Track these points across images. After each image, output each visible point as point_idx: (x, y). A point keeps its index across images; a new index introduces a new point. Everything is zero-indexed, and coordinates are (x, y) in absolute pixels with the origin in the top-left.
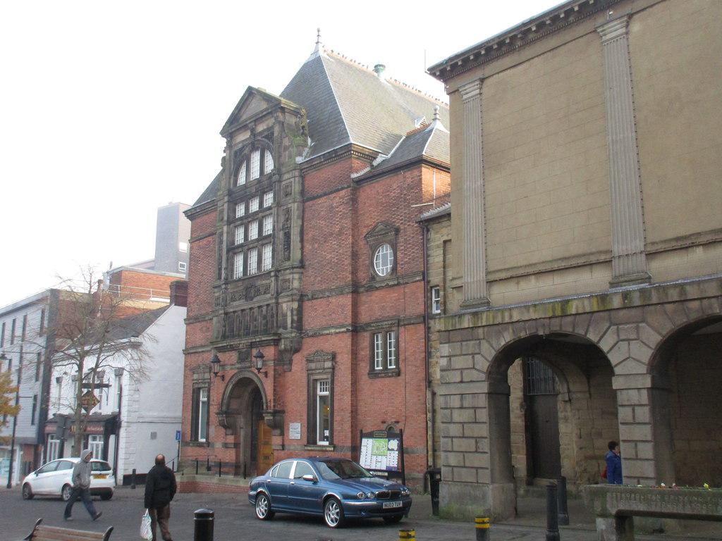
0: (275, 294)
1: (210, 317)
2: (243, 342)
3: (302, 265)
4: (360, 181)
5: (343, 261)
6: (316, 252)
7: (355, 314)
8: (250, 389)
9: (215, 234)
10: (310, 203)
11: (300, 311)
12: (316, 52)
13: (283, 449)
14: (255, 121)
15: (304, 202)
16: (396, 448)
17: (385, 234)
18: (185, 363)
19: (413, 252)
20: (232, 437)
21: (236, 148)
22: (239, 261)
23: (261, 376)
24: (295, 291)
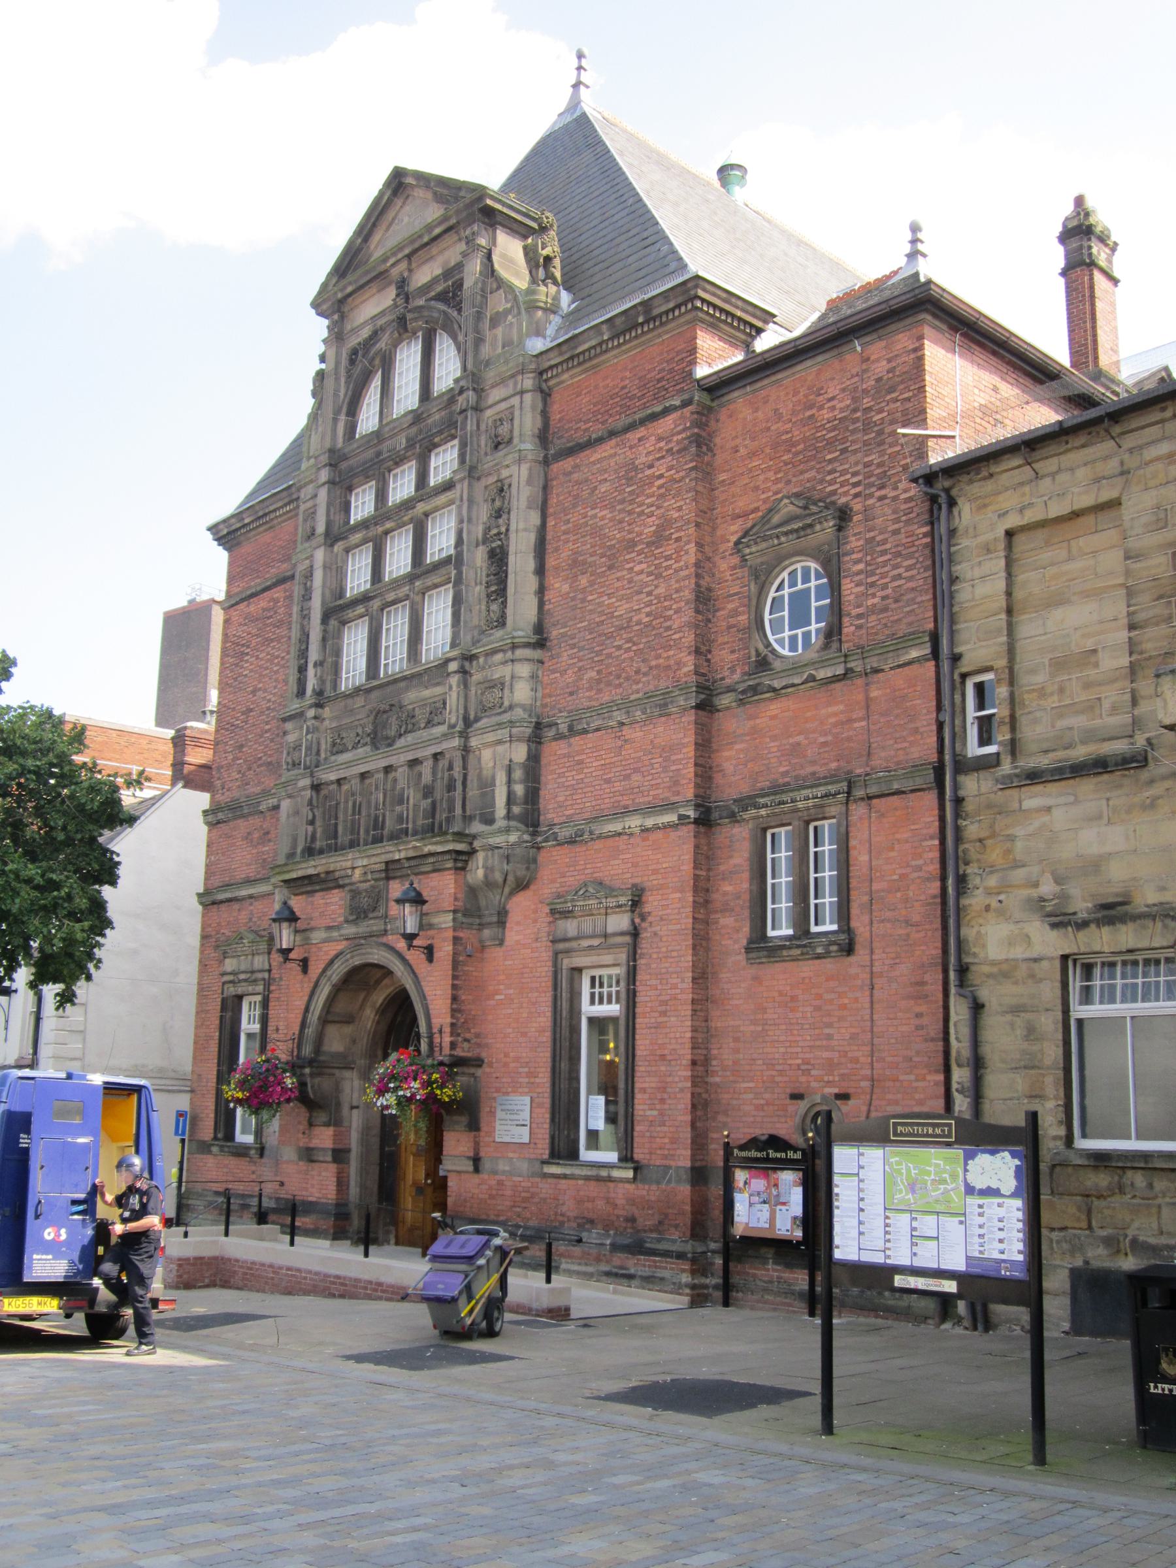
0: (461, 723)
1: (273, 802)
2: (359, 863)
3: (541, 643)
4: (721, 386)
5: (669, 618)
6: (583, 600)
7: (705, 772)
8: (379, 997)
9: (292, 577)
10: (567, 464)
11: (533, 768)
12: (575, 103)
13: (477, 1170)
14: (409, 257)
15: (546, 462)
16: (1009, 1183)
17: (803, 528)
18: (203, 929)
19: (899, 576)
20: (330, 1131)
21: (353, 341)
22: (355, 642)
23: (416, 957)
24: (519, 713)
